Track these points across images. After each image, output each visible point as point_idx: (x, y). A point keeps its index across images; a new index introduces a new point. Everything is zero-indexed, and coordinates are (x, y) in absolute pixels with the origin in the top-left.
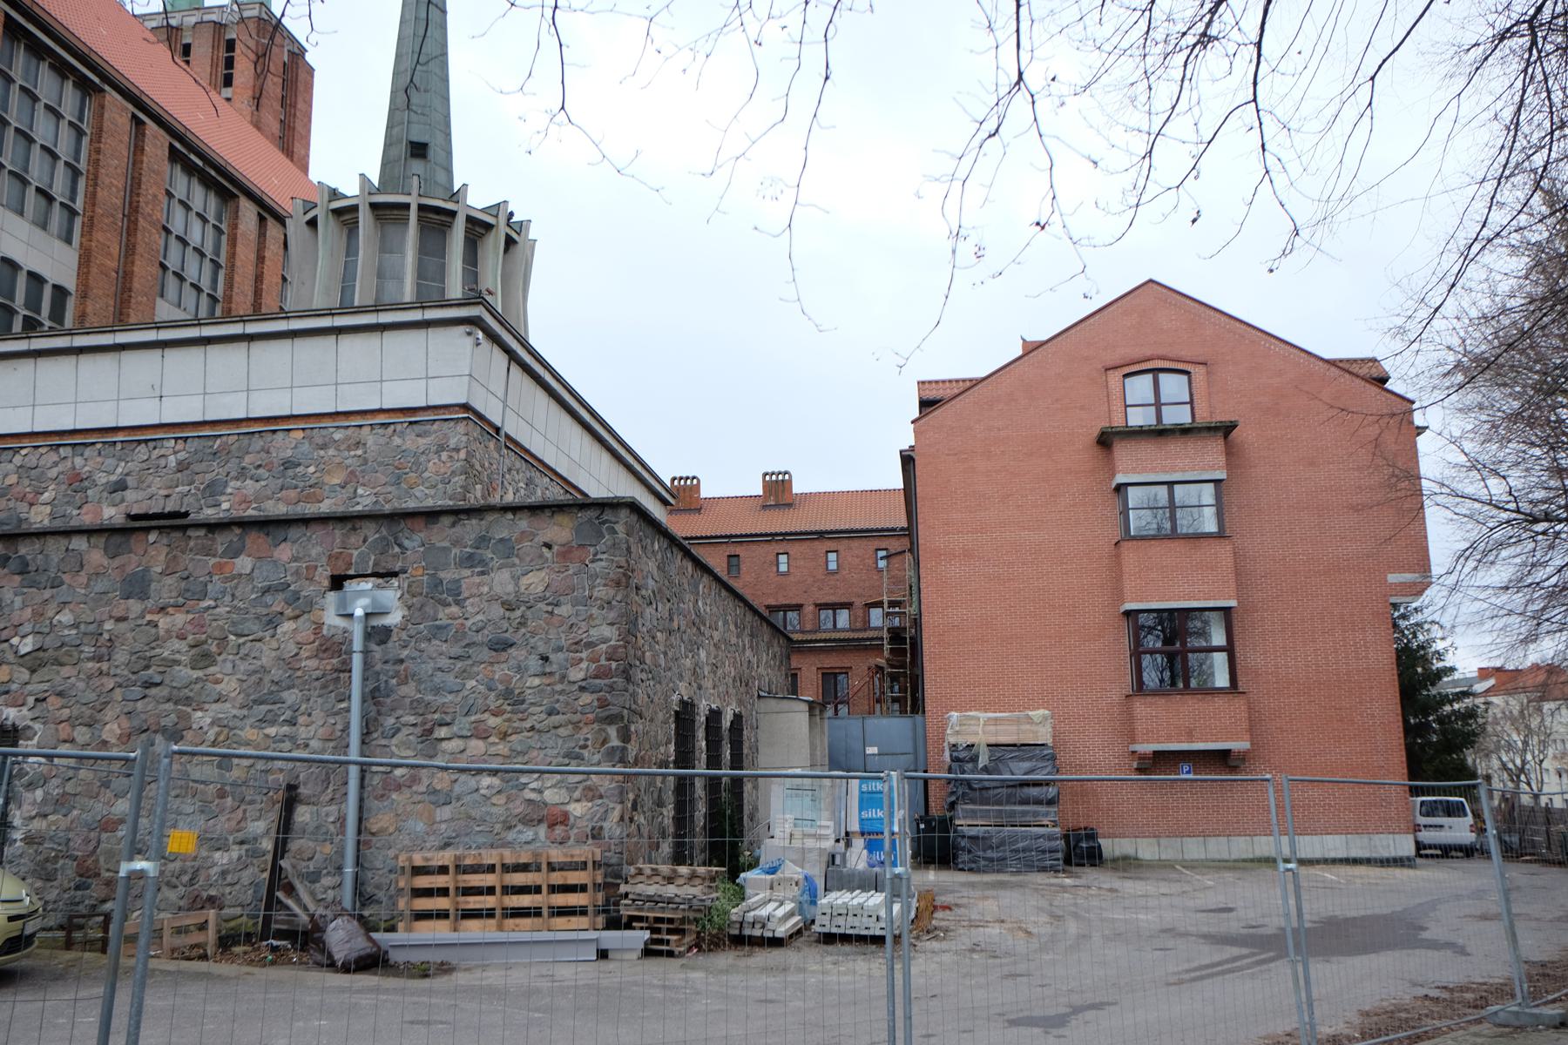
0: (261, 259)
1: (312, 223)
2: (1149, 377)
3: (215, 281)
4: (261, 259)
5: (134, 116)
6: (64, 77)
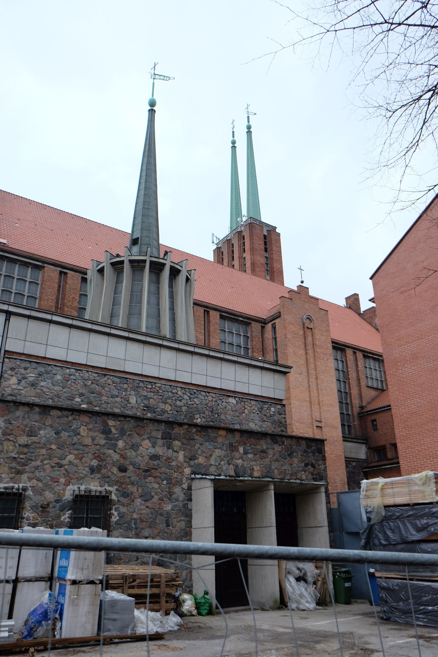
0: (358, 371)
1: (101, 271)
2: (8, 339)
3: (345, 387)
4: (358, 371)
5: (353, 352)
6: (225, 320)
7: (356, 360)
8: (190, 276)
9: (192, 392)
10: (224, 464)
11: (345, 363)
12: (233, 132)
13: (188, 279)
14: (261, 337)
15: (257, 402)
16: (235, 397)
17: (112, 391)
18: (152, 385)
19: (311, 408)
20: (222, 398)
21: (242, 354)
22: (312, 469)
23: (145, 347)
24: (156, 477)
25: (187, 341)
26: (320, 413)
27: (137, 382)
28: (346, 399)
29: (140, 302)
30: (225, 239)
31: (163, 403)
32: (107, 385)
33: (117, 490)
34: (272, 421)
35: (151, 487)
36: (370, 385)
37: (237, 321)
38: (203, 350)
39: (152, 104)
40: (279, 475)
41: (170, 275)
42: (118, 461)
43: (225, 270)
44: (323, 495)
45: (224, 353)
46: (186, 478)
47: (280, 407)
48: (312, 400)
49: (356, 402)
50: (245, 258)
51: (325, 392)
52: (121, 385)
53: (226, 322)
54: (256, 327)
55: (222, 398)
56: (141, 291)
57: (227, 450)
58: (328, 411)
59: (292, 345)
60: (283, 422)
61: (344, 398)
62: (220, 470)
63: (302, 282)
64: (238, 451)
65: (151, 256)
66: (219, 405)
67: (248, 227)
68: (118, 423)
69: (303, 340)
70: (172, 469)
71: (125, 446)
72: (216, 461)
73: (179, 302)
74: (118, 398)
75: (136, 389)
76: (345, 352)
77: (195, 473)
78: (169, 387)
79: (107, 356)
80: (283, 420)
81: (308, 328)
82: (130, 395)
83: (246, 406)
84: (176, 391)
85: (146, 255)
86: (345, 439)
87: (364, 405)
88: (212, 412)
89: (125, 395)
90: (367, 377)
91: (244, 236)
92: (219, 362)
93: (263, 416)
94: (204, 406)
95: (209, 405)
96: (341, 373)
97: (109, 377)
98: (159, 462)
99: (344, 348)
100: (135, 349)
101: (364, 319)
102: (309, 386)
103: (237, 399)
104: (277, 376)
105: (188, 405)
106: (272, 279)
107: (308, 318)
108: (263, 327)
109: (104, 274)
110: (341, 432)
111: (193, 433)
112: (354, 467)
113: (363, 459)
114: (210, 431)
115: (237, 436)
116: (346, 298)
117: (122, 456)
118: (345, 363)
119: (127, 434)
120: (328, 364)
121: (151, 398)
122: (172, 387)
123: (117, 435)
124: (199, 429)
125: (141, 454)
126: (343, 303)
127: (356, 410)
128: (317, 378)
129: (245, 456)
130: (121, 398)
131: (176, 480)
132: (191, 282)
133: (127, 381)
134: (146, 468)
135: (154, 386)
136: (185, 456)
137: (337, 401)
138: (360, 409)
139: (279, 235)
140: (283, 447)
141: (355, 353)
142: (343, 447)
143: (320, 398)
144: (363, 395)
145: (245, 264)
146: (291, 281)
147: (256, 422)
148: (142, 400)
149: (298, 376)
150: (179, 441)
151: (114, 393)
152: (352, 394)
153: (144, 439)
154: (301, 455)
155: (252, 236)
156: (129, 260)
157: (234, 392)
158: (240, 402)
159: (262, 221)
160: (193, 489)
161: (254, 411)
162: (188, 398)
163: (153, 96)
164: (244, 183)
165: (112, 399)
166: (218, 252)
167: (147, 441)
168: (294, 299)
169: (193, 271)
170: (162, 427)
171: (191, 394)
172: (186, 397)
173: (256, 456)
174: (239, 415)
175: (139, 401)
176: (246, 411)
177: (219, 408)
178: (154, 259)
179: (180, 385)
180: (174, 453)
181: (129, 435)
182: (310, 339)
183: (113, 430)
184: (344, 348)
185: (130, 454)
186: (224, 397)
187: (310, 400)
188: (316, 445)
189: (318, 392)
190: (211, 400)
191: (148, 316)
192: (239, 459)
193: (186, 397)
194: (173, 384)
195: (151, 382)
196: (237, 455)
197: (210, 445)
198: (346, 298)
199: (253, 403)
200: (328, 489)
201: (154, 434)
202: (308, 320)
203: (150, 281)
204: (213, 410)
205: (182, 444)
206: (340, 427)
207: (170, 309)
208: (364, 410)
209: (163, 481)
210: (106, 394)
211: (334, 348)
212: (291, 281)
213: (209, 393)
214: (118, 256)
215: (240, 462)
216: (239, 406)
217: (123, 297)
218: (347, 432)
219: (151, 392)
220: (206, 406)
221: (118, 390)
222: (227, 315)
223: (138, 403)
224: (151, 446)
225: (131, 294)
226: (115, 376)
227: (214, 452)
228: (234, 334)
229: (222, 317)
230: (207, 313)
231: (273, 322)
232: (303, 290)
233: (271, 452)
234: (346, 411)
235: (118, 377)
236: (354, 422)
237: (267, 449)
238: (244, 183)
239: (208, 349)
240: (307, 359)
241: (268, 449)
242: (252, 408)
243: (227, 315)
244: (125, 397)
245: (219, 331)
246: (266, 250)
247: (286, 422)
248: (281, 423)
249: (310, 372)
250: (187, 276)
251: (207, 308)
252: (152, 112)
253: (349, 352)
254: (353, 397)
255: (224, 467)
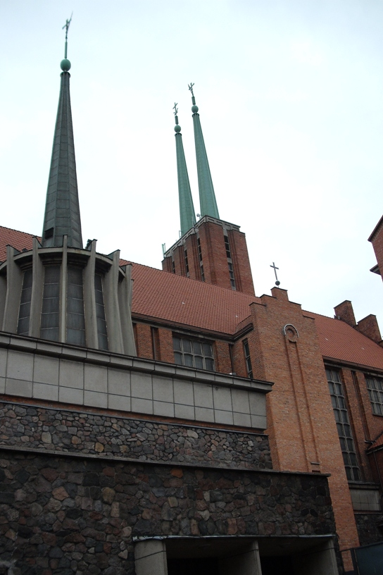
3: (345, 418)
5: (352, 371)
7: (356, 382)
8: (125, 272)
9: (134, 425)
10: (183, 518)
11: (342, 386)
12: (176, 117)
13: (121, 278)
14: (229, 358)
15: (228, 435)
16: (195, 428)
17: (15, 427)
18: (74, 417)
19: (304, 447)
20: (177, 431)
21: (205, 368)
22: (312, 518)
23: (62, 364)
24: (78, 543)
25: (123, 353)
26: (317, 453)
27: (53, 412)
28: (348, 434)
29: (57, 309)
30: (176, 246)
31: (92, 441)
32: (8, 419)
33: (17, 565)
34: (250, 460)
35: (70, 558)
36: (377, 413)
37: (195, 340)
38: (149, 365)
39: (66, 66)
40: (265, 529)
41: (96, 271)
42: (17, 520)
43: (178, 278)
44: (333, 553)
45: (175, 368)
46: (125, 542)
47: (261, 440)
48: (304, 436)
49: (361, 436)
50: (202, 267)
51: (320, 425)
52: (29, 418)
53: (182, 342)
54: (222, 346)
55: (177, 431)
56: (58, 295)
57: (185, 498)
58: (327, 449)
59: (271, 366)
60: (267, 461)
61: (346, 431)
62: (177, 527)
63: (278, 283)
64: (202, 498)
65: (68, 247)
66: (173, 440)
67: (202, 227)
68: (15, 463)
69: (286, 359)
70: (102, 530)
71: (27, 497)
72: (169, 515)
73: (111, 307)
74: (24, 437)
75: (50, 422)
76: (342, 373)
77: (139, 534)
78: (99, 418)
79: (6, 378)
80: (266, 457)
81: (290, 342)
82: (43, 431)
83: (213, 441)
84: (111, 424)
85: (62, 247)
86: (352, 487)
87: (372, 438)
88: (164, 451)
89: (36, 432)
90: (372, 403)
91: (199, 240)
92: (169, 383)
93: (238, 454)
94: (151, 443)
95: (159, 442)
96: (338, 400)
97: (10, 407)
98: (82, 520)
99: (340, 367)
100: (46, 367)
101: (360, 332)
102: (299, 419)
103: (199, 431)
104: (253, 398)
105: (129, 443)
106: (239, 289)
107: (289, 329)
108: (231, 346)
109: (6, 278)
110: (346, 476)
111: (133, 475)
112: (366, 522)
113: (377, 511)
114: (157, 470)
115: (200, 476)
116: (335, 308)
117: (22, 512)
118: (342, 386)
119: (29, 480)
120: (321, 385)
121: (73, 435)
122: (104, 418)
123: (15, 482)
124: (141, 469)
125: (53, 508)
126: (331, 314)
127: (362, 447)
128: (308, 407)
129: (213, 505)
130: (30, 436)
131: (109, 545)
132: (126, 281)
133: (38, 412)
134: (62, 530)
135: (77, 418)
136: (121, 509)
137: (337, 436)
138: (367, 445)
139: (243, 235)
140: (269, 488)
141: (354, 373)
142: (350, 497)
143: (315, 434)
144: (369, 427)
145: (203, 275)
146: (262, 287)
147: (228, 462)
148: (60, 438)
149: (282, 406)
150: (110, 487)
151: (18, 430)
152: (355, 426)
153: (57, 486)
154: (296, 500)
155: (210, 239)
156: (40, 255)
157: (194, 422)
158: (203, 435)
159: (221, 219)
160: (136, 557)
161: (225, 447)
162: (128, 433)
163: (66, 57)
164: (194, 179)
165: (15, 438)
166: (167, 261)
167: (62, 489)
168: (268, 306)
169: (128, 266)
170: (84, 467)
171: (132, 427)
172: (125, 431)
173: (230, 505)
174: (203, 453)
175: (56, 439)
176: (213, 448)
177: (174, 445)
178: (73, 251)
179: (116, 415)
180: (104, 505)
181: (33, 480)
182: (293, 355)
183: (8, 474)
184: (340, 367)
185: (36, 508)
186: (180, 429)
187: (302, 436)
188: (315, 483)
189: (311, 427)
190: (161, 434)
191: (68, 328)
192: (204, 510)
193: (125, 431)
194: (105, 414)
195: (72, 413)
196: (201, 504)
197: (158, 491)
198: (335, 308)
199: (223, 435)
200: (338, 545)
201: (72, 478)
202: (289, 332)
203: (69, 283)
204: (165, 448)
205: (117, 492)
206: (344, 469)
207: (98, 317)
208: (373, 446)
209: (89, 548)
210: (7, 431)
211: (327, 368)
212: (262, 287)
213: (158, 424)
214: (25, 251)
215: (206, 514)
216: (203, 441)
217: (32, 304)
218: (353, 477)
219: (73, 426)
220: (154, 443)
221: (24, 425)
222: (182, 332)
223: (55, 442)
224: (68, 496)
225: (44, 300)
226: (20, 406)
227: (167, 501)
228: (194, 358)
229: (175, 336)
230: (154, 331)
231: (244, 338)
232: (279, 294)
233: (251, 498)
234: (350, 450)
235: (24, 407)
236: (361, 462)
237: (245, 494)
238: (194, 179)
239: (152, 363)
240: (292, 382)
241: (246, 493)
242: (221, 443)
243: (182, 332)
244: (35, 434)
245: (173, 354)
246: (228, 255)
247: (271, 460)
248: (263, 461)
249: (298, 399)
250: (120, 272)
251: (155, 325)
252: (65, 76)
253: (347, 373)
254: (356, 430)
255: (182, 522)
